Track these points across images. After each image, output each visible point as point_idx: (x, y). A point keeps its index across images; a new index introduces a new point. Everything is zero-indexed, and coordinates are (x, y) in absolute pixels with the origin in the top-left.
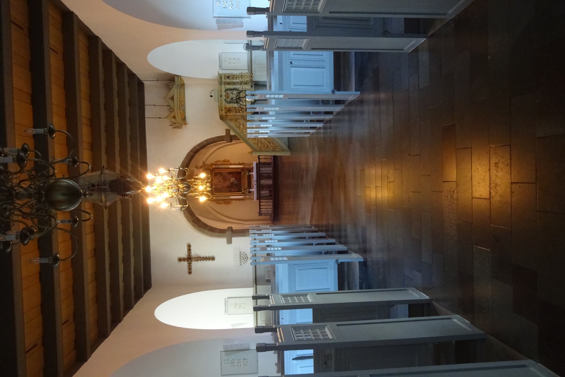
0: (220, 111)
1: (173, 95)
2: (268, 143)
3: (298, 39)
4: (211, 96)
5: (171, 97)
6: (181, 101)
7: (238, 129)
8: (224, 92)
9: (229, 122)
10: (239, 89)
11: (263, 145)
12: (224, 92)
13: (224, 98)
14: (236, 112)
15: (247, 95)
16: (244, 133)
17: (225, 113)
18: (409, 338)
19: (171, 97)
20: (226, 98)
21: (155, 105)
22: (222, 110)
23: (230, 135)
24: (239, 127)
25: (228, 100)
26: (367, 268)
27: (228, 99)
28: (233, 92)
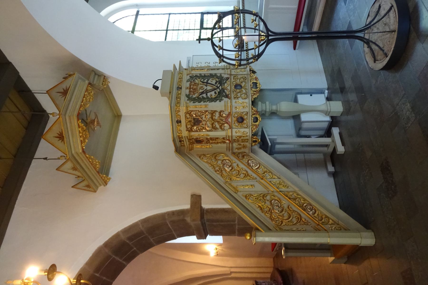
0: (175, 124)
1: (68, 87)
2: (299, 210)
3: (414, 121)
4: (156, 88)
5: (62, 91)
6: (84, 101)
7: (219, 176)
8: (187, 81)
9: (197, 160)
10: (223, 75)
11: (286, 216)
12: (187, 81)
13: (185, 91)
14: (214, 128)
15: (208, 39)
16: (233, 184)
17: (187, 130)
18: (39, 146)
19: (62, 91)
20: (190, 92)
21: (46, 159)
22: (179, 122)
23: (201, 207)
24: (221, 171)
25: (194, 96)
26: (390, 18)
27: (194, 94)
28: (207, 81)
